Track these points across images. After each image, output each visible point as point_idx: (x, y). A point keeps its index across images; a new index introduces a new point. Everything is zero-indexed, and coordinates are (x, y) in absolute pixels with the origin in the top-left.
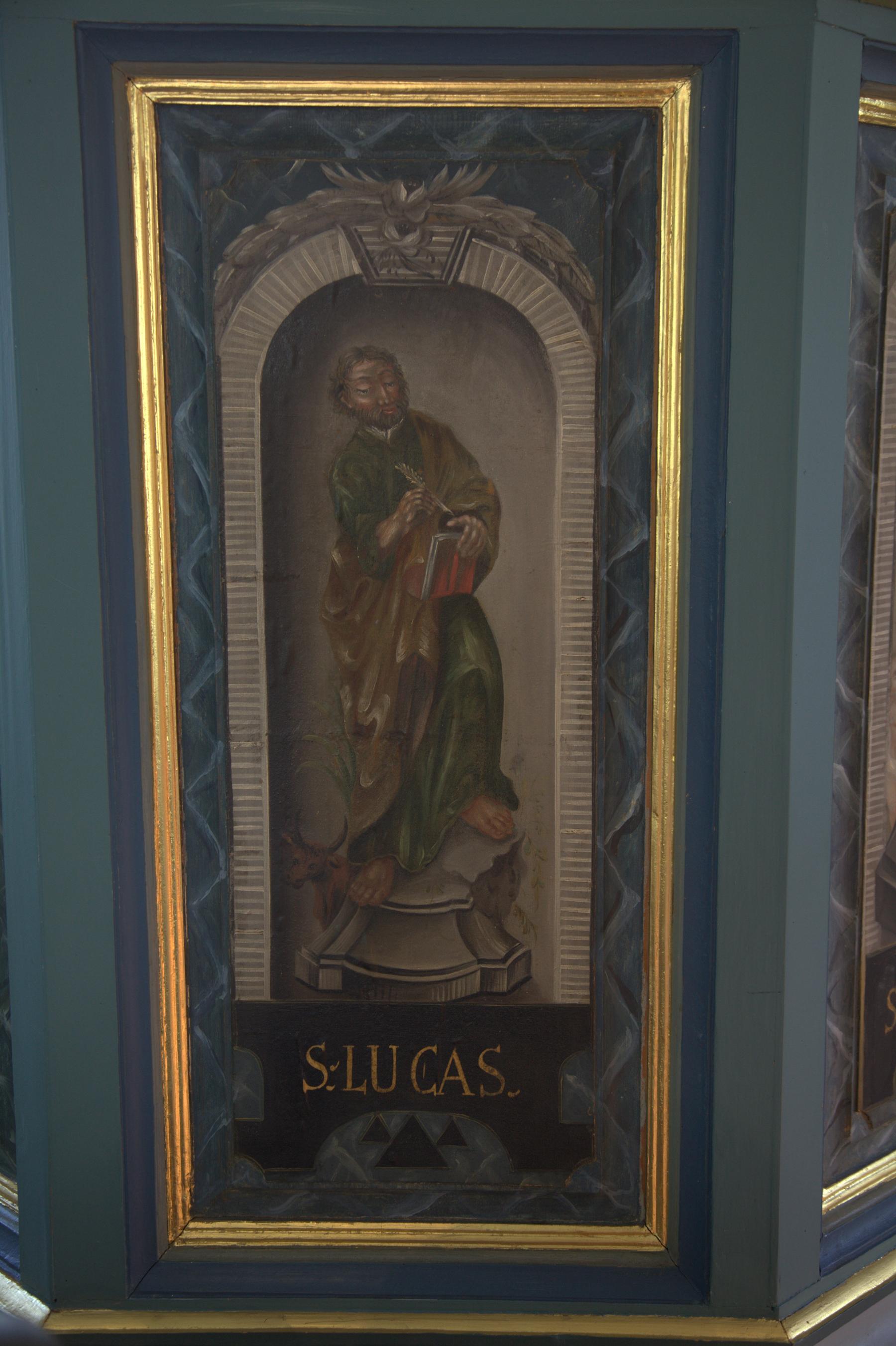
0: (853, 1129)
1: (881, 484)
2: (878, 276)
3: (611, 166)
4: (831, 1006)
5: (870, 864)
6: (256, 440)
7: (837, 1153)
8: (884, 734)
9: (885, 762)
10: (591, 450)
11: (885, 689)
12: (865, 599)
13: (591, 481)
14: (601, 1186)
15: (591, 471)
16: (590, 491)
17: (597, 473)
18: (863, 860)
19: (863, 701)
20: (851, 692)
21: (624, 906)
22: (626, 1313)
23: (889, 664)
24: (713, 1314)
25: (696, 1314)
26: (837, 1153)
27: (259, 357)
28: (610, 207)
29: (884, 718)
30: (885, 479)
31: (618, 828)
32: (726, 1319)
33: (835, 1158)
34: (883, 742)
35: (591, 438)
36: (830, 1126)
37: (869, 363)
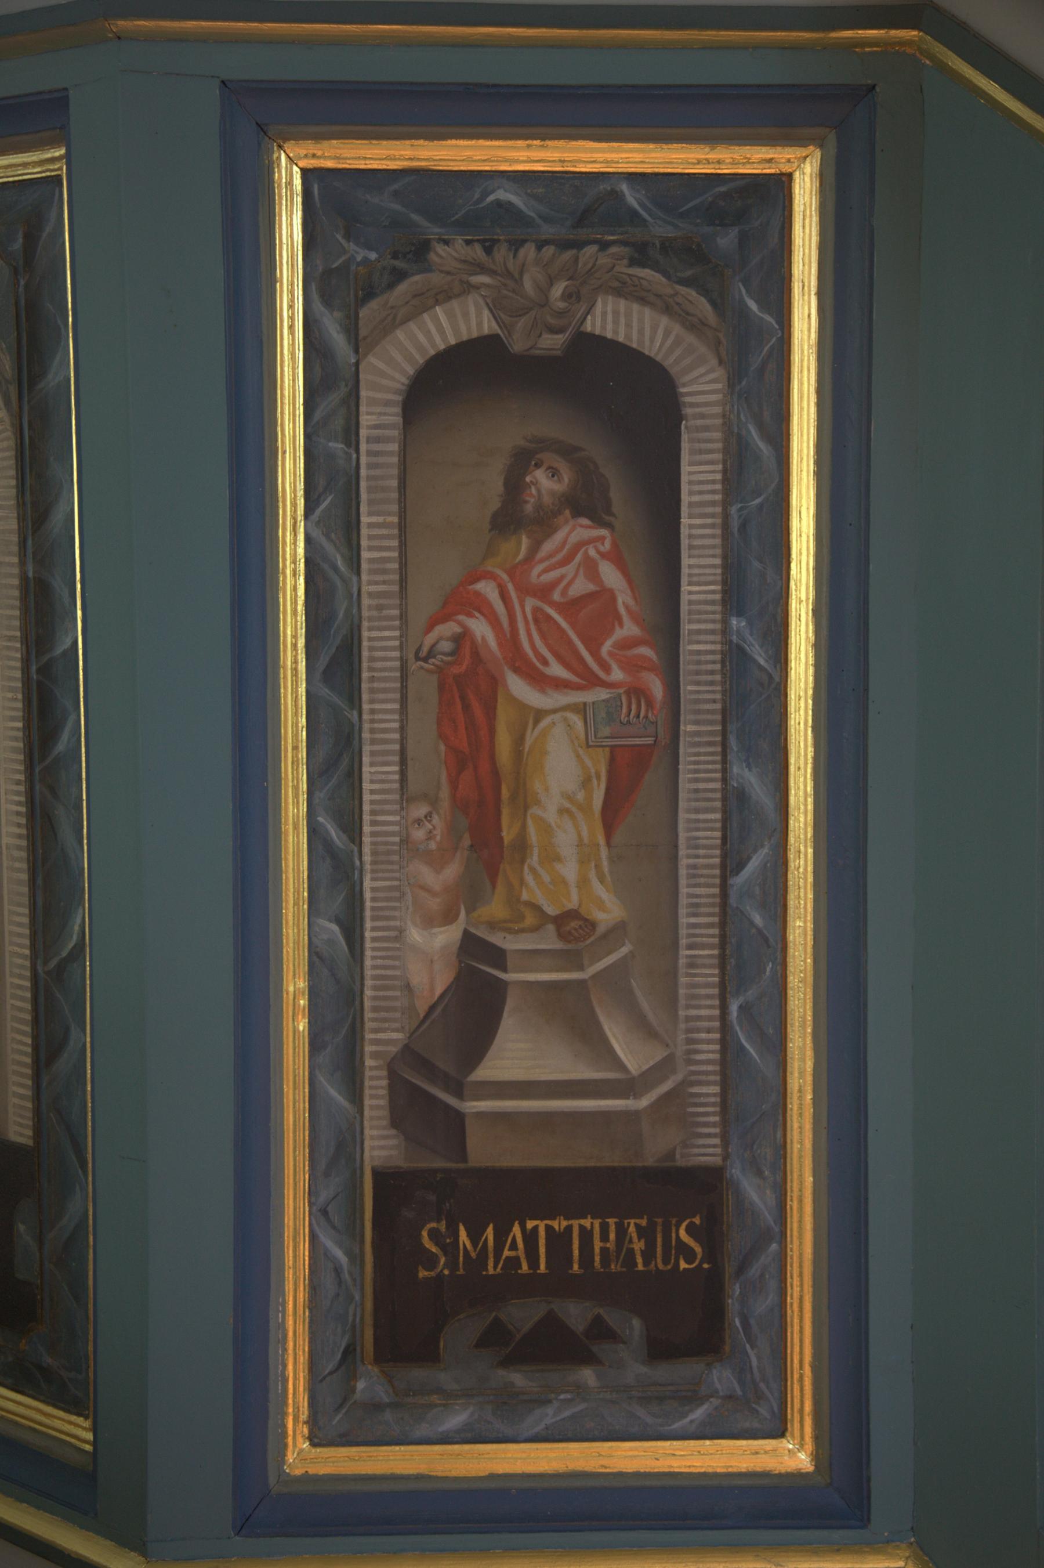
0: (361, 1385)
1: (365, 589)
2: (349, 343)
3: (21, 240)
4: (328, 1220)
5: (375, 1055)
6: (687, 608)
7: (344, 1411)
8: (397, 894)
9: (401, 931)
10: (15, 538)
11: (397, 839)
12: (353, 725)
13: (16, 571)
14: (50, 1360)
15: (16, 560)
16: (16, 582)
17: (22, 563)
18: (362, 1047)
19: (356, 849)
20: (344, 837)
21: (72, 1043)
22: (38, 1508)
23: (402, 809)
24: (98, 1532)
25: (87, 1529)
26: (344, 1411)
27: (369, 492)
28: (22, 282)
29: (397, 875)
30: (369, 583)
31: (64, 954)
32: (108, 1543)
33: (340, 1416)
34: (397, 904)
35: (14, 525)
36: (331, 1373)
37: (346, 444)
